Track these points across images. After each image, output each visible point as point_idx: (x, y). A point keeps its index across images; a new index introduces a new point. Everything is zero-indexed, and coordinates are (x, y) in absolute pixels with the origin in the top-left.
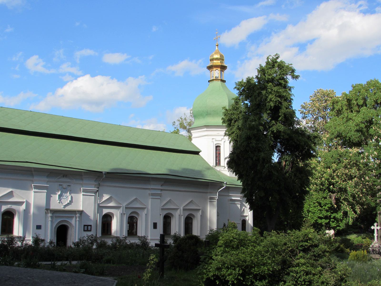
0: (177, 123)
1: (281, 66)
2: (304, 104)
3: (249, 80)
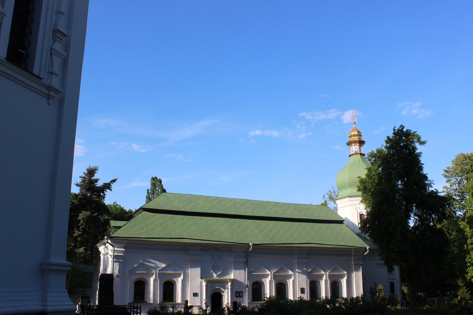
0: (327, 196)
1: (408, 134)
2: (447, 169)
3: (379, 151)
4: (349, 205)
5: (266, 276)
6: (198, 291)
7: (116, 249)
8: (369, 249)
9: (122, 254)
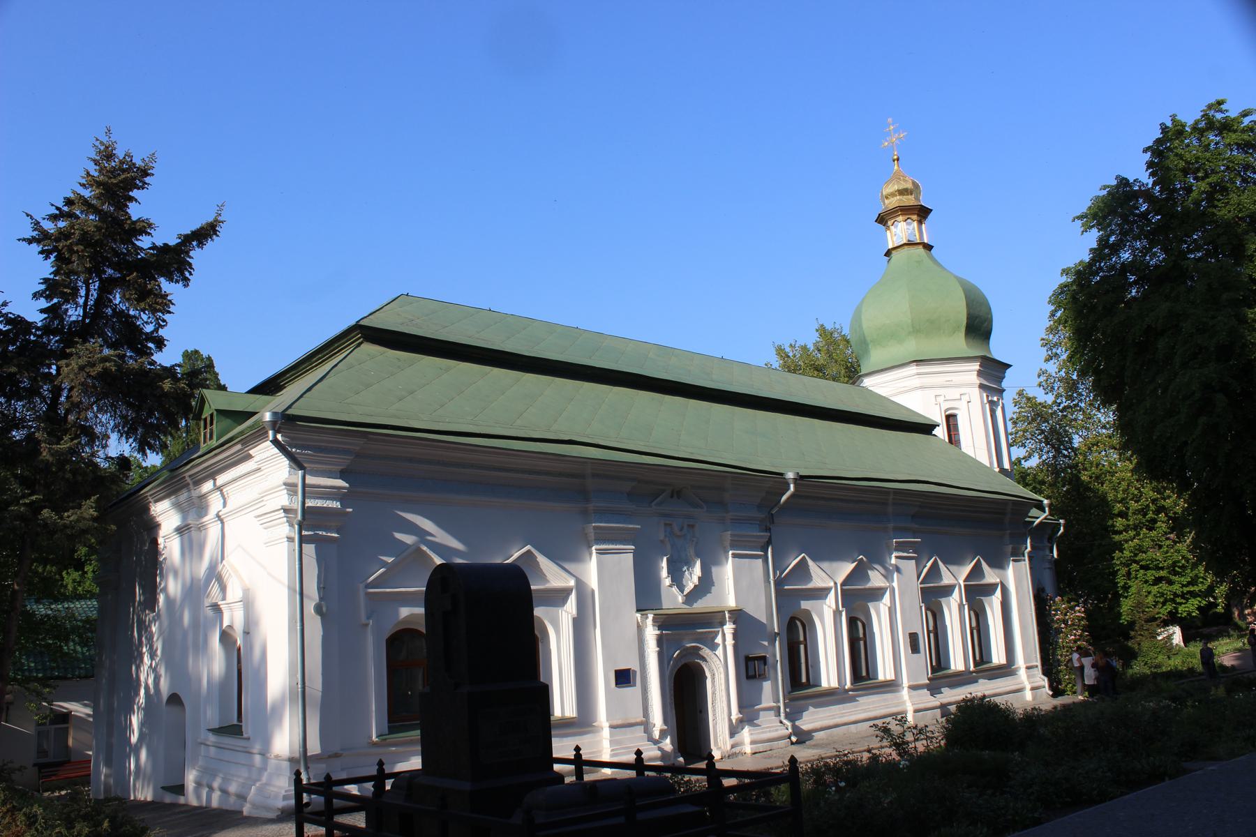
4: (917, 388)
5: (820, 593)
6: (632, 664)
7: (310, 480)
9: (336, 505)
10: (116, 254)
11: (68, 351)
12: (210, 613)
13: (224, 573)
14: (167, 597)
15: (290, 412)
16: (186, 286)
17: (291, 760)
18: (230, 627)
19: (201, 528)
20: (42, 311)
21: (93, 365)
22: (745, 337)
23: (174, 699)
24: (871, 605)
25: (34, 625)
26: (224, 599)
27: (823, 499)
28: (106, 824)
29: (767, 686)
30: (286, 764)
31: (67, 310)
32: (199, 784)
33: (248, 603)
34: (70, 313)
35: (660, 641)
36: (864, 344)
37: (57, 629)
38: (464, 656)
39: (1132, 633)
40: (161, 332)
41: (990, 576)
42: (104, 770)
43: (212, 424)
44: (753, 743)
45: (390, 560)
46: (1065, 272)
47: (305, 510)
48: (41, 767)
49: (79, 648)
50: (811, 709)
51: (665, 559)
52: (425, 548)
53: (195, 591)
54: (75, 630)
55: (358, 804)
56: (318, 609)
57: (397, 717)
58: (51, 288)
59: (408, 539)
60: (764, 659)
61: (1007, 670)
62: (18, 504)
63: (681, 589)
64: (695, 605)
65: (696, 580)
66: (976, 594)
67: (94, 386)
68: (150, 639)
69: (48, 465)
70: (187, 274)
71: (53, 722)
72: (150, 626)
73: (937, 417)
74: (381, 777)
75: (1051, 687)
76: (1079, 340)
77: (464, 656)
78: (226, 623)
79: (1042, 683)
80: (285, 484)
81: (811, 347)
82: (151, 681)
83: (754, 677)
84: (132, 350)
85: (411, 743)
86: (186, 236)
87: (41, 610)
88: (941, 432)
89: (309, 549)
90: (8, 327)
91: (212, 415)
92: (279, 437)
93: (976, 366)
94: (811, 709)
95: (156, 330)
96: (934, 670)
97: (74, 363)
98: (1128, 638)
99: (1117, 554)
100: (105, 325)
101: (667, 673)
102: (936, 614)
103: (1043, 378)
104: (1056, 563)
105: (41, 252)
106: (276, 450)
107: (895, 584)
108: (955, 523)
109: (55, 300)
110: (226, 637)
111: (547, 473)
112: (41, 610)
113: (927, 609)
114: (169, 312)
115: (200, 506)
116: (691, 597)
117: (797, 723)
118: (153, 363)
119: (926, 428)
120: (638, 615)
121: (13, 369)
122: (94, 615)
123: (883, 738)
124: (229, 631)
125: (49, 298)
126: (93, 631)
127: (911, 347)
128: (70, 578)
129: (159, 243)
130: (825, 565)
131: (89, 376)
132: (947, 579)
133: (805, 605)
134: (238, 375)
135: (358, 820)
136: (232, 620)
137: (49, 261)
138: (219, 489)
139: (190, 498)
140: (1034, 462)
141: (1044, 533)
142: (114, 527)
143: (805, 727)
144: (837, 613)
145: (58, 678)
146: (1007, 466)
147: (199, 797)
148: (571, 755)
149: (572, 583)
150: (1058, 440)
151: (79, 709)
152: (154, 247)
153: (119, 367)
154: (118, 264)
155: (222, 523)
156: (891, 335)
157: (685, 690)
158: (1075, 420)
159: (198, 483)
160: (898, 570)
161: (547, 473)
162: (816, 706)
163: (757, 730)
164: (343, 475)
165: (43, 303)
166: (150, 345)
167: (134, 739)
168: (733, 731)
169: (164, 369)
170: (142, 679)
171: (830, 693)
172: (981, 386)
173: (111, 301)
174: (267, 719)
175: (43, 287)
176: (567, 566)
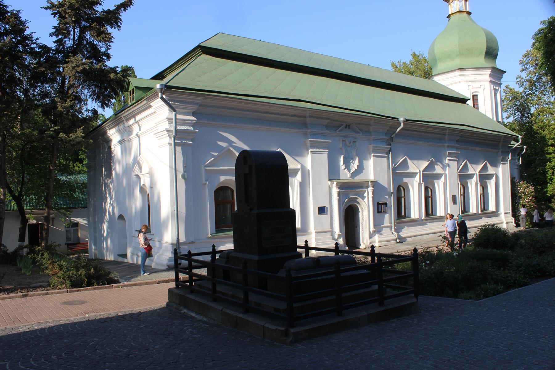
5: (412, 175)
6: (326, 204)
7: (179, 117)
8: (522, 139)
9: (191, 128)
10: (86, 14)
11: (67, 60)
12: (134, 179)
13: (140, 161)
14: (116, 173)
15: (168, 84)
16: (119, 30)
17: (172, 244)
18: (144, 185)
19: (130, 141)
20: (55, 42)
21: (79, 66)
22: (380, 58)
23: (121, 217)
24: (435, 181)
25: (61, 186)
26: (141, 172)
27: (416, 131)
28: (92, 270)
29: (387, 216)
30: (170, 246)
31: (66, 41)
32: (133, 254)
33: (151, 174)
34: (67, 43)
35: (339, 194)
36: (435, 60)
37: (71, 187)
38: (256, 196)
39: (553, 200)
40: (109, 52)
41: (491, 170)
42: (93, 247)
43: (133, 93)
44: (379, 242)
45: (216, 154)
46: (543, 22)
47: (177, 131)
48: (68, 245)
49: (81, 196)
50: (406, 227)
51: (342, 156)
52: (232, 149)
53: (128, 170)
54: (78, 187)
55: (203, 265)
56: (183, 177)
57: (220, 225)
58: (58, 31)
59: (224, 145)
60: (386, 204)
61: (495, 214)
62: (49, 131)
63: (349, 171)
64: (355, 178)
65: (356, 167)
66: (484, 178)
67: (79, 76)
68: (110, 191)
69: (61, 113)
70: (119, 24)
71: (72, 227)
72: (109, 185)
73: (468, 95)
74: (214, 252)
75: (515, 223)
76: (546, 58)
77: (256, 196)
78: (142, 184)
79: (511, 221)
80: (167, 118)
81: (408, 63)
82: (111, 210)
83: (381, 212)
84: (96, 60)
85: (229, 237)
86: (118, 6)
87: (63, 178)
88: (470, 103)
89: (179, 149)
90: (40, 50)
91: (133, 89)
92: (164, 96)
93: (489, 72)
94: (406, 227)
95: (107, 51)
96: (462, 212)
97: (70, 66)
98: (550, 202)
99: (548, 163)
100: (83, 48)
101: (342, 209)
102: (465, 187)
103: (518, 80)
104: (521, 166)
105: (52, 14)
106: (163, 103)
107: (447, 172)
108: (477, 144)
109: (60, 37)
110: (142, 190)
111: (288, 115)
112: (63, 178)
113: (461, 184)
114: (112, 42)
115: (128, 131)
116: (354, 175)
117: (400, 234)
118: (106, 66)
119: (464, 101)
120: (329, 182)
121: (43, 69)
122: (86, 181)
123: (444, 242)
124: (144, 187)
125: (57, 36)
126: (86, 188)
127: (458, 62)
128: (78, 167)
129: (106, 9)
130: (415, 162)
131: (77, 72)
132: (471, 171)
133: (405, 180)
134: (143, 74)
135: (203, 272)
136: (144, 181)
137: (56, 18)
138: (137, 122)
139: (124, 127)
140: (511, 119)
141: (516, 152)
142: (91, 141)
143: (403, 236)
144: (420, 184)
145: (73, 208)
146: (500, 120)
147: (132, 259)
148: (303, 244)
149: (299, 166)
150: (524, 109)
151: (82, 221)
152: (104, 11)
153: (90, 68)
154: (88, 19)
155: (139, 138)
156: (448, 56)
157: (350, 216)
158: (533, 100)
159: (128, 120)
160: (448, 165)
161: (288, 115)
162: (408, 226)
163: (382, 236)
164: (194, 114)
165: (55, 38)
166: (104, 57)
167: (105, 234)
168: (371, 236)
169: (111, 68)
170: (107, 208)
171: (415, 221)
172: (491, 82)
173: (85, 37)
174: (162, 226)
175: (54, 30)
176: (297, 158)
